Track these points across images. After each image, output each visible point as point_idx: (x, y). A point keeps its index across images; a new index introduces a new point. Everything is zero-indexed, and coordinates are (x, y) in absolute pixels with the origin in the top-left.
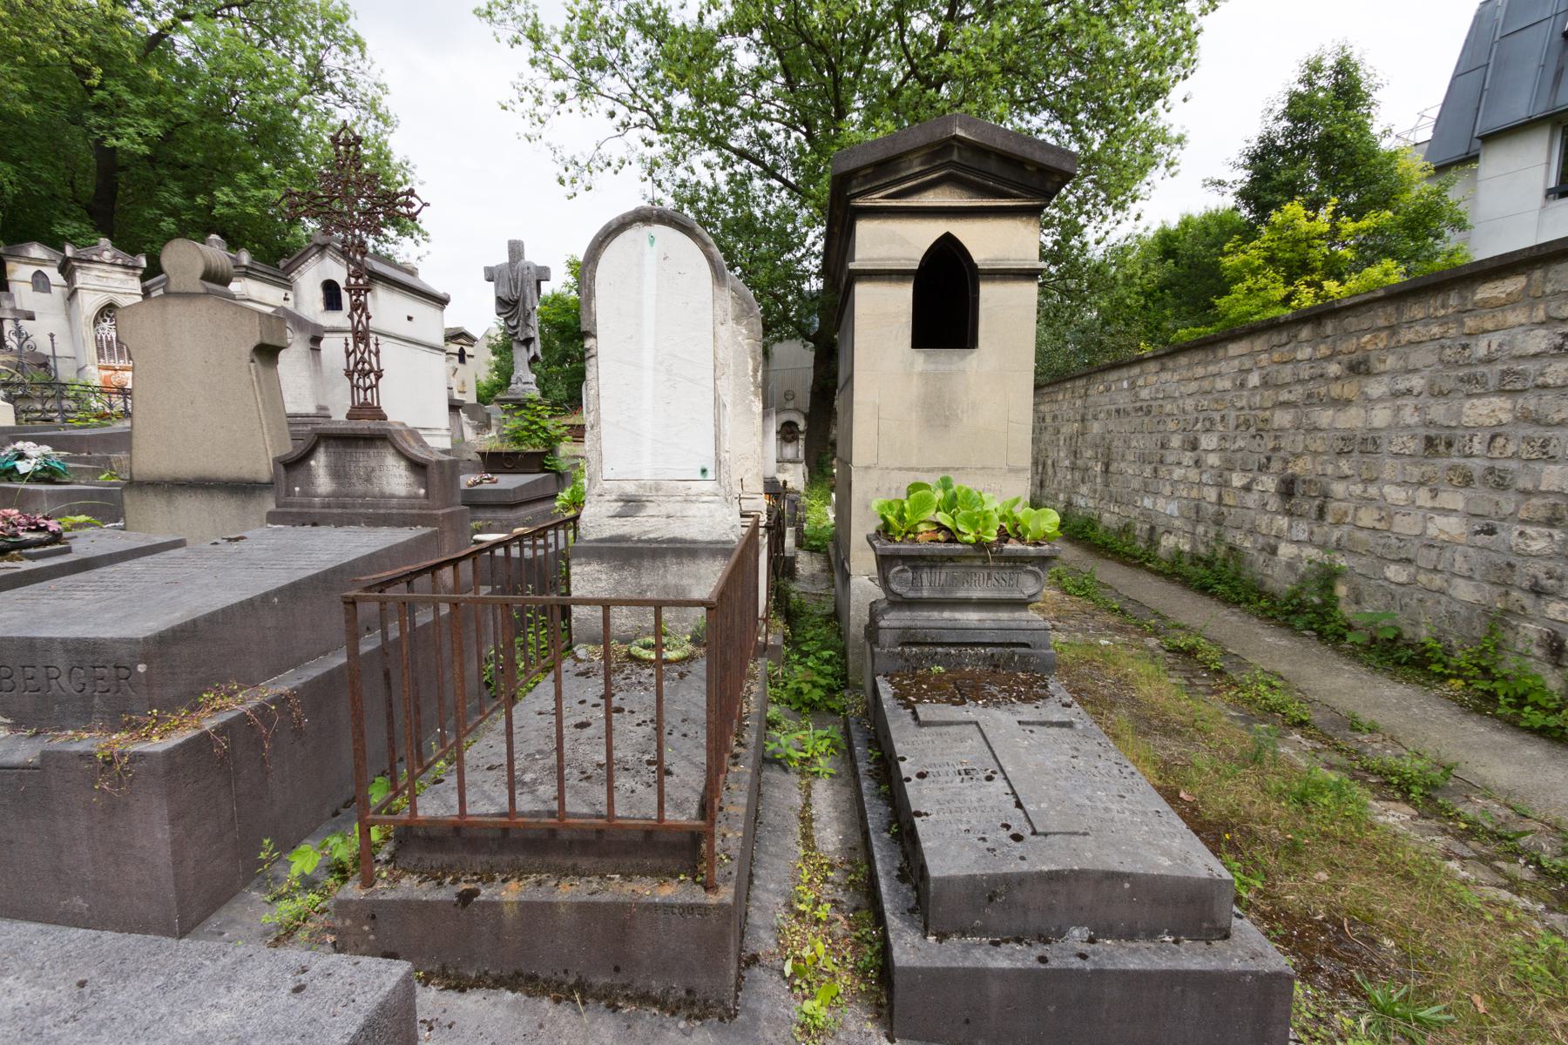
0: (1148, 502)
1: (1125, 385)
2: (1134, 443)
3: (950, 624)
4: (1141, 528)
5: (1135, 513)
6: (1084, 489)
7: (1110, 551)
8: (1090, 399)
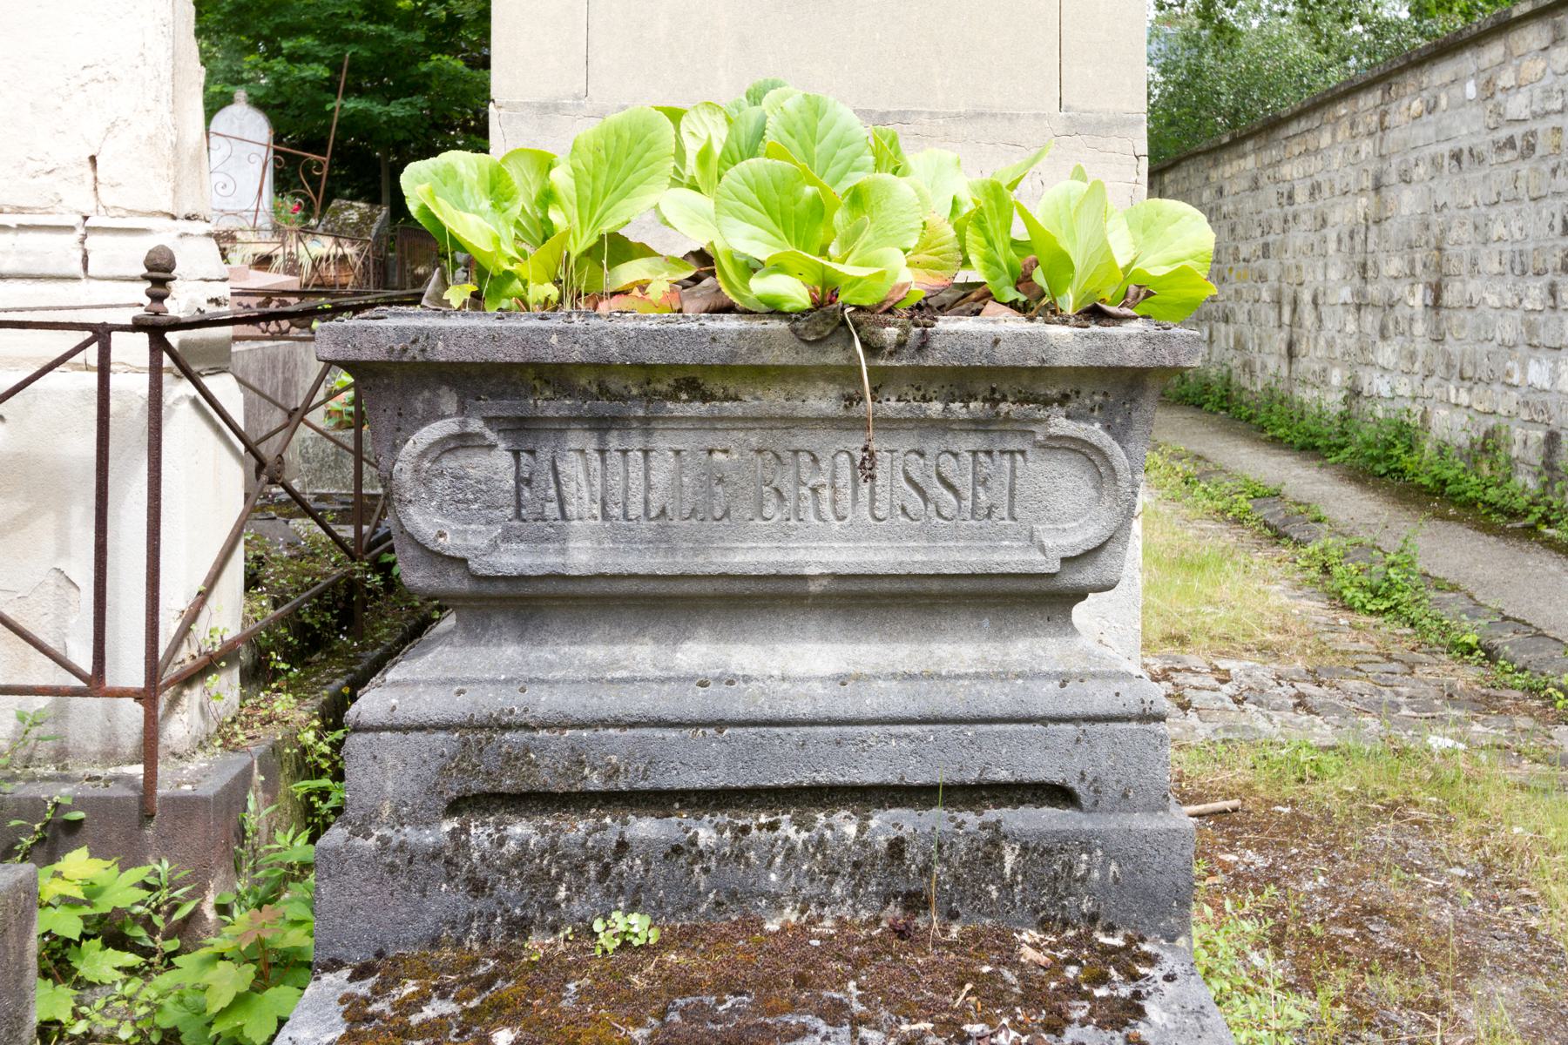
0: (1538, 373)
1: (1471, 90)
2: (1497, 230)
3: (694, 703)
4: (1525, 441)
5: (1507, 402)
6: (1386, 354)
7: (1451, 499)
8: (1393, 136)
